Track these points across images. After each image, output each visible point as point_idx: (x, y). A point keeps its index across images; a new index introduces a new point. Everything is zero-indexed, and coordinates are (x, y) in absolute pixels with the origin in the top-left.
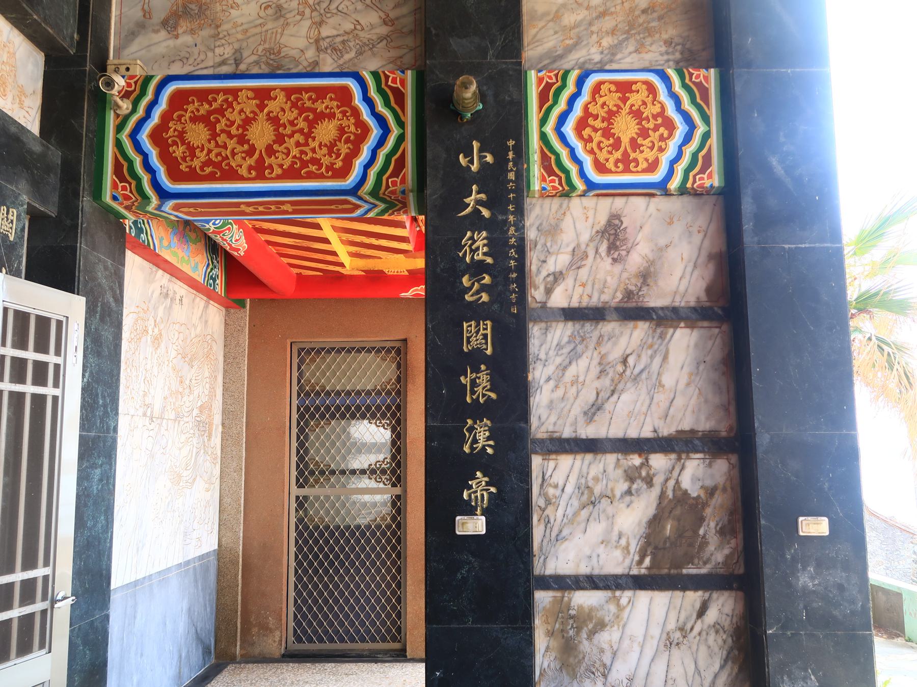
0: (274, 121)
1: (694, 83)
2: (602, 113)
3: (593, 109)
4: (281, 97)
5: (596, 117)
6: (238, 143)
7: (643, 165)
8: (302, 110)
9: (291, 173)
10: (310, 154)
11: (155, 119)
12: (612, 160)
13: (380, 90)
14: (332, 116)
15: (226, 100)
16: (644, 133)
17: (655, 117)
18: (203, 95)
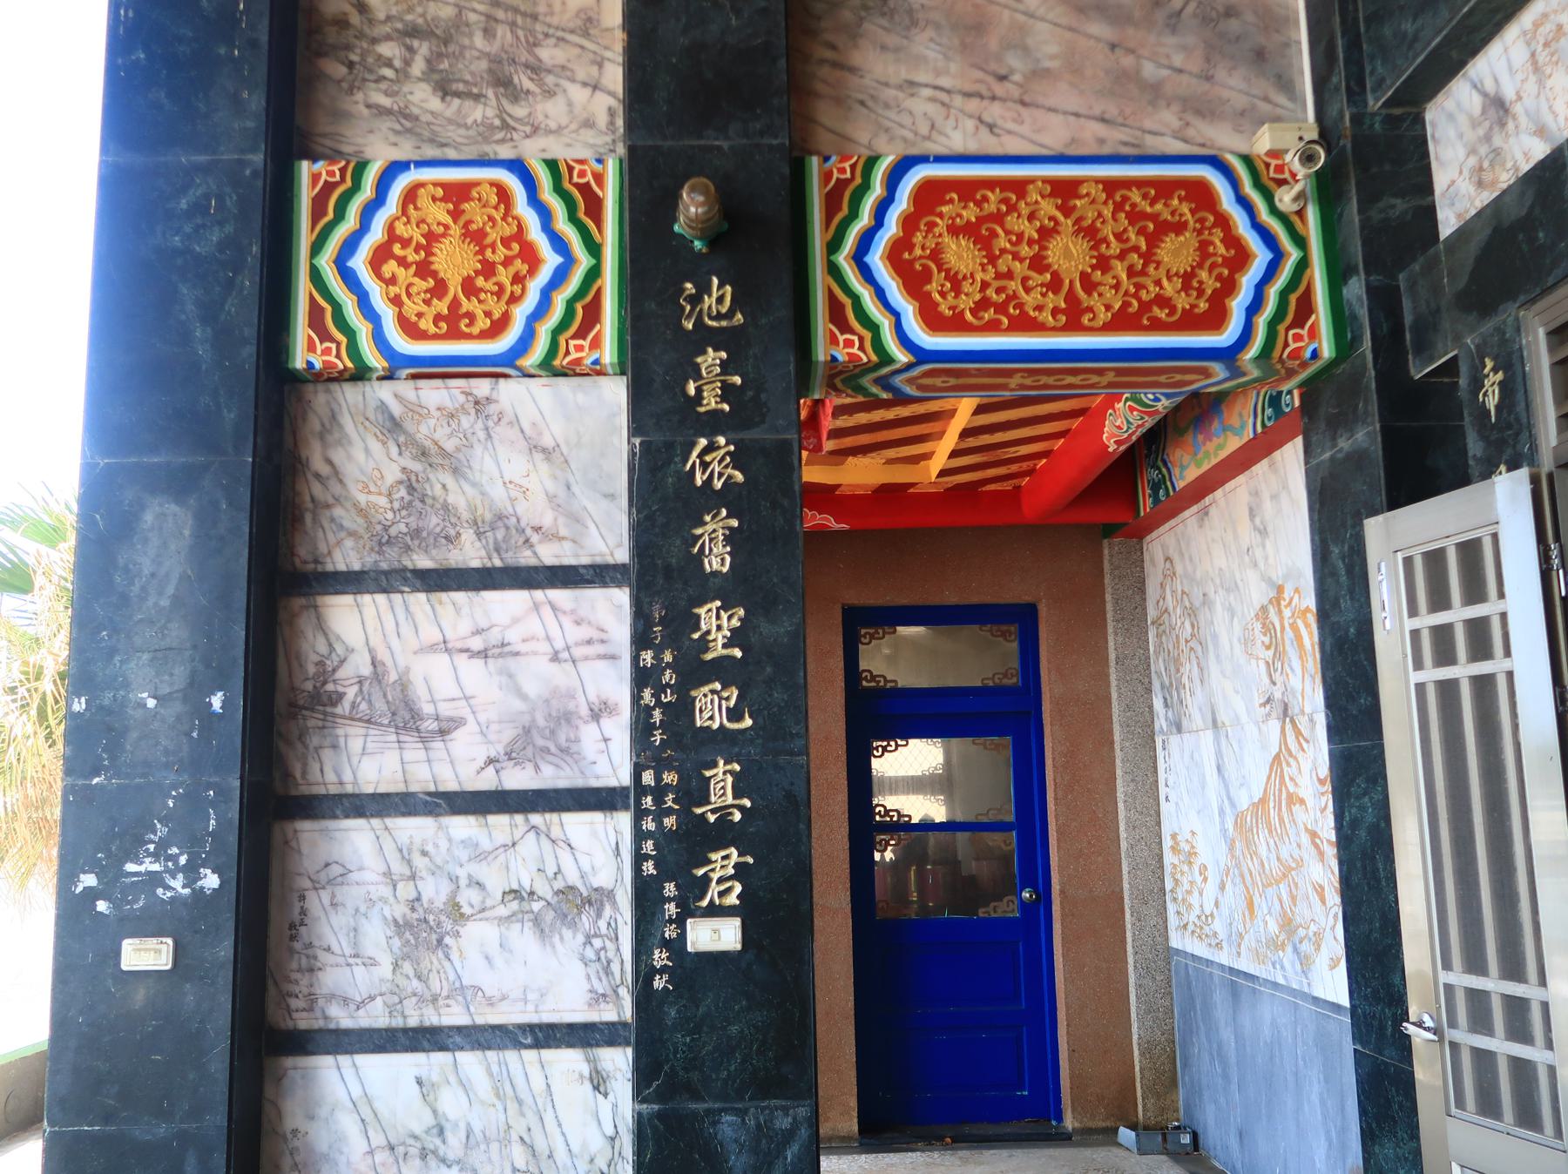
0: (1090, 233)
1: (577, 185)
2: (1030, 231)
3: (400, 229)
4: (1098, 192)
5: (406, 243)
6: (415, 275)
7: (483, 323)
8: (1135, 216)
9: (1122, 321)
10: (1154, 290)
11: (892, 227)
12: (430, 313)
13: (558, 189)
14: (1180, 228)
15: (1005, 201)
16: (488, 270)
17: (506, 242)
18: (968, 190)
